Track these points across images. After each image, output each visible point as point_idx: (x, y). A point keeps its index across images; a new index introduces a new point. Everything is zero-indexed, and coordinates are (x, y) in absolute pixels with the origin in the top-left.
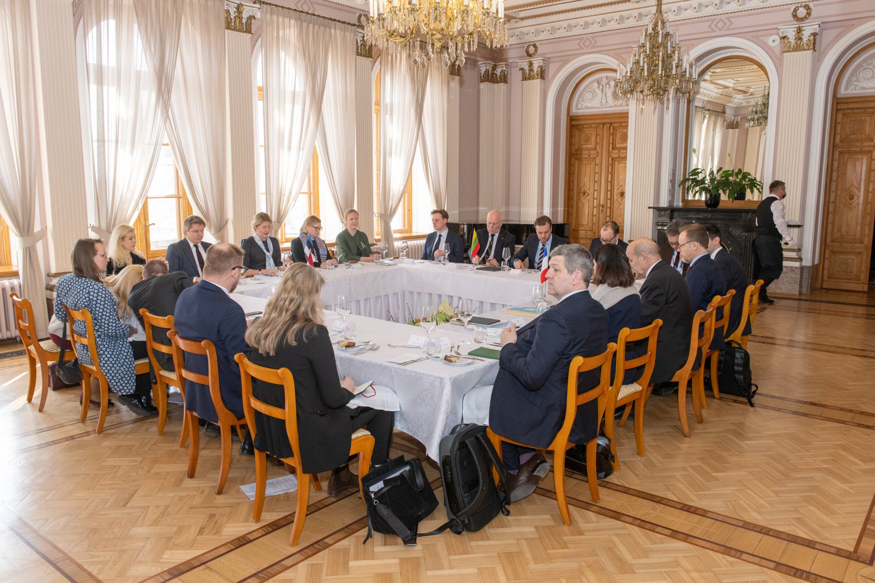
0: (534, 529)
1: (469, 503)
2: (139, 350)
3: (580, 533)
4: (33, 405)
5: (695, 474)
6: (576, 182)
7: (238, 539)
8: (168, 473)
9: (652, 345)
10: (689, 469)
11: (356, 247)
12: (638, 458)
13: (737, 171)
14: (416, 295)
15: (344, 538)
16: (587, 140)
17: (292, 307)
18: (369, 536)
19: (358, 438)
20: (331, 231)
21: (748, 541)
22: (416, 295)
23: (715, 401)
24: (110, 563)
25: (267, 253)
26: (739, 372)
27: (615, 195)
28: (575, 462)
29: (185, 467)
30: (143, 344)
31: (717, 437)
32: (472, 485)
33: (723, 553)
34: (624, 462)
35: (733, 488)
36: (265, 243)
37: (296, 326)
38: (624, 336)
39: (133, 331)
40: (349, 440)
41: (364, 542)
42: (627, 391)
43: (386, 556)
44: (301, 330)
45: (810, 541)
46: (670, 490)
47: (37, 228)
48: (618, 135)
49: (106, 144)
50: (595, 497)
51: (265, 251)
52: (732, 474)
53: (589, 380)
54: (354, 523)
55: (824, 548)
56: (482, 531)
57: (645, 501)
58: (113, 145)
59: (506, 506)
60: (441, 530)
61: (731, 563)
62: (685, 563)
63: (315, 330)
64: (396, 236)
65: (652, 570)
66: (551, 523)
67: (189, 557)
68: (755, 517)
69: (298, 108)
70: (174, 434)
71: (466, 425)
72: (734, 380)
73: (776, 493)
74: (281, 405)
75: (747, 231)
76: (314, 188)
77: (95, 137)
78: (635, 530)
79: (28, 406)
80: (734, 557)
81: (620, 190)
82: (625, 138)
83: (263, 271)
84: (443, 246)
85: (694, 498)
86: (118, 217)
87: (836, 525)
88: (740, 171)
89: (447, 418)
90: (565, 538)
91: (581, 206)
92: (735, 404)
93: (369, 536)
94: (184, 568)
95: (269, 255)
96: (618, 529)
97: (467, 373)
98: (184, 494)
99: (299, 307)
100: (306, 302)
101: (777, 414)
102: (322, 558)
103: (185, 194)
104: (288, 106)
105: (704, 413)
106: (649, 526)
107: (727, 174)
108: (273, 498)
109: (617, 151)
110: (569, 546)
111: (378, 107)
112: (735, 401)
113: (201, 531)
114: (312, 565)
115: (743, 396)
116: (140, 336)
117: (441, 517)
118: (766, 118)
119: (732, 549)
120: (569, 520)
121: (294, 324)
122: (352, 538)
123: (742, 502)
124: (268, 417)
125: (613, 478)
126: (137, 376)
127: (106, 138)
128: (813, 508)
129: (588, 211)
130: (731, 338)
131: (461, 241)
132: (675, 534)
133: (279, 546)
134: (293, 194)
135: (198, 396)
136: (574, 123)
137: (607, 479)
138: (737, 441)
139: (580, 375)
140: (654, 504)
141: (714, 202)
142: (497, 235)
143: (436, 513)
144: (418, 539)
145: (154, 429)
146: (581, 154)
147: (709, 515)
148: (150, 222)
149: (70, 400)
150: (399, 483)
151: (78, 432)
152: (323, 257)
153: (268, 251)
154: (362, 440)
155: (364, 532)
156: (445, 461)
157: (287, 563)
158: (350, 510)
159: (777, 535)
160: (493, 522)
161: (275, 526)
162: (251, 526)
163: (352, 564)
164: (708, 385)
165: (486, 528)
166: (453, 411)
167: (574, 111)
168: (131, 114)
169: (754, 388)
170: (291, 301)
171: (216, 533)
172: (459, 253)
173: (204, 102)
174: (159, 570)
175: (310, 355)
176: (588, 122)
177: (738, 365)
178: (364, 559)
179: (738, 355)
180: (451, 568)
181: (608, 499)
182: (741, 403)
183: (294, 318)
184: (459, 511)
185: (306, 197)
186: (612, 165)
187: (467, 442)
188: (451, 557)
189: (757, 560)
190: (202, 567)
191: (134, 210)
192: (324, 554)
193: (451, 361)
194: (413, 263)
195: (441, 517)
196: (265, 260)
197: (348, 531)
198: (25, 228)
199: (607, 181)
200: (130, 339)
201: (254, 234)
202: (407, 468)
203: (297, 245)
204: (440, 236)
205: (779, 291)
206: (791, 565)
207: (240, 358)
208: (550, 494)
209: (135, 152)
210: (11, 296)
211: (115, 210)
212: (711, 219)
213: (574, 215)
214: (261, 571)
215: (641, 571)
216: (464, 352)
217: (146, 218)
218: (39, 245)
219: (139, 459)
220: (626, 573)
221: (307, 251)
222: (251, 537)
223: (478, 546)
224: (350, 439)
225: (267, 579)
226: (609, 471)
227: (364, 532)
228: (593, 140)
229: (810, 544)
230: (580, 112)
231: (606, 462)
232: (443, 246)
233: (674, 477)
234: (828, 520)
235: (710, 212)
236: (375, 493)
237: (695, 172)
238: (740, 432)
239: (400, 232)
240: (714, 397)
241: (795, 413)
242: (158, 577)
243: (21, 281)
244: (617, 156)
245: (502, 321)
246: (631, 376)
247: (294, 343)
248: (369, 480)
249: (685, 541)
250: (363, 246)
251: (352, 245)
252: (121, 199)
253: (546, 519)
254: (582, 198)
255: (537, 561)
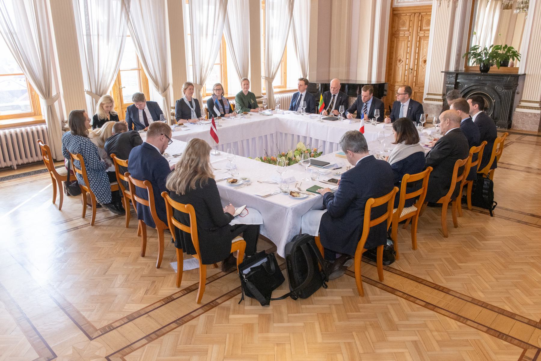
0: (341, 298)
1: (302, 282)
2: (112, 177)
3: (369, 302)
4: (56, 205)
5: (446, 263)
6: (394, 53)
7: (167, 298)
8: (130, 253)
9: (426, 183)
10: (444, 260)
11: (248, 102)
12: (412, 251)
13: (503, 46)
14: (284, 135)
15: (227, 300)
16: (404, 25)
17: (194, 164)
18: (243, 298)
19: (236, 242)
20: (234, 89)
21: (473, 311)
22: (284, 135)
23: (468, 211)
24: (95, 311)
25: (192, 109)
26: (485, 194)
27: (416, 71)
28: (370, 256)
29: (140, 249)
30: (114, 173)
31: (465, 238)
32: (304, 272)
33: (455, 320)
34: (403, 254)
35: (469, 275)
36: (191, 102)
37: (197, 177)
38: (406, 179)
39: (108, 166)
40: (230, 244)
41: (239, 303)
42: (406, 212)
43: (250, 312)
44: (199, 180)
45: (512, 314)
46: (429, 275)
47: (54, 93)
48: (425, 21)
49: (92, 37)
50: (381, 278)
51: (190, 107)
52: (470, 264)
53: (377, 212)
54: (235, 290)
55: (521, 319)
56: (309, 298)
57: (412, 282)
58: (96, 37)
59: (326, 282)
60: (284, 297)
61: (459, 326)
62: (430, 325)
63: (207, 181)
64: (275, 90)
65: (409, 329)
66: (352, 294)
67: (139, 309)
68: (480, 296)
69: (212, 7)
70: (135, 227)
71: (303, 235)
72: (482, 197)
73: (496, 279)
74: (188, 224)
75: (507, 89)
76: (223, 61)
77: (85, 33)
78: (403, 301)
79: (53, 205)
80: (462, 322)
81: (424, 59)
82: (428, 23)
83: (190, 121)
84: (302, 102)
85: (444, 281)
86: (102, 84)
87: (532, 303)
88: (506, 46)
89: (290, 232)
90: (360, 305)
91: (397, 68)
92: (481, 214)
93: (243, 298)
94: (135, 316)
95: (193, 110)
96: (392, 300)
97: (303, 204)
98: (139, 267)
99: (197, 164)
100: (202, 160)
101: (507, 222)
102: (214, 312)
103: (142, 67)
104: (205, 6)
105: (459, 220)
106: (412, 299)
107: (497, 48)
108: (188, 272)
109: (423, 32)
110: (361, 310)
111: (264, 5)
112: (481, 212)
113: (146, 293)
114: (208, 316)
115: (487, 209)
116: (112, 168)
117: (285, 289)
118: (528, 7)
119: (462, 317)
120: (362, 293)
121: (195, 175)
122: (232, 300)
123: (473, 285)
124: (182, 231)
125: (394, 265)
126: (112, 192)
127: (91, 33)
128: (518, 291)
129: (402, 73)
130: (482, 171)
131: (314, 97)
132: (428, 305)
133: (190, 303)
134: (210, 67)
135: (144, 211)
136: (395, 12)
137: (390, 266)
138: (478, 241)
139: (373, 210)
140: (418, 284)
141: (485, 69)
142: (337, 95)
143: (283, 285)
144: (271, 302)
145: (124, 223)
146: (399, 34)
147: (451, 293)
148: (123, 86)
149: (76, 203)
150: (260, 270)
151: (80, 224)
152: (227, 111)
153: (192, 107)
154: (238, 243)
155: (239, 296)
156: (288, 257)
157: (194, 314)
158: (232, 281)
159: (492, 308)
160: (317, 292)
161: (189, 290)
162: (175, 290)
163: (231, 316)
164: (464, 200)
165: (312, 296)
166: (294, 226)
167: (393, 6)
168: (106, 18)
169: (494, 204)
170: (192, 160)
171: (154, 294)
172: (311, 109)
173: (151, 6)
174: (122, 316)
175: (205, 195)
176: (405, 12)
177: (485, 189)
178: (238, 314)
179: (485, 183)
180: (289, 322)
181: (390, 279)
182: (485, 213)
183: (195, 172)
184: (296, 287)
185: (219, 66)
186: (419, 41)
187: (302, 247)
188: (289, 315)
189: (476, 325)
190: (146, 315)
191: (111, 80)
192: (215, 309)
193: (293, 196)
194: (283, 114)
195: (285, 289)
196: (190, 114)
197: (230, 295)
198: (47, 94)
199: (415, 52)
200: (107, 171)
201: (184, 96)
202: (265, 260)
203: (211, 103)
204: (301, 95)
205: (524, 129)
206: (497, 329)
207: (164, 195)
208: (352, 274)
209: (110, 43)
210: (39, 141)
211: (100, 80)
212: (483, 80)
213: (392, 75)
214: (179, 319)
215: (403, 329)
216: (304, 188)
217: (120, 84)
218: (56, 104)
219: (114, 243)
220: (393, 330)
221: (219, 107)
222: (175, 297)
223: (306, 308)
224: (231, 244)
225: (182, 324)
226: (392, 261)
227: (239, 296)
228: (407, 24)
229: (512, 316)
230: (400, 5)
231: (390, 256)
232: (302, 102)
233: (433, 265)
234: (528, 300)
235: (483, 75)
236: (246, 275)
237: (475, 48)
238: (482, 234)
239: (279, 87)
240: (467, 208)
241: (519, 221)
242: (121, 321)
243: (47, 125)
244: (423, 35)
245: (331, 163)
246: (409, 203)
247: (194, 187)
248: (243, 266)
249: (433, 310)
250: (252, 101)
251: (246, 101)
252: (103, 74)
253: (348, 292)
254: (398, 63)
255: (340, 320)
